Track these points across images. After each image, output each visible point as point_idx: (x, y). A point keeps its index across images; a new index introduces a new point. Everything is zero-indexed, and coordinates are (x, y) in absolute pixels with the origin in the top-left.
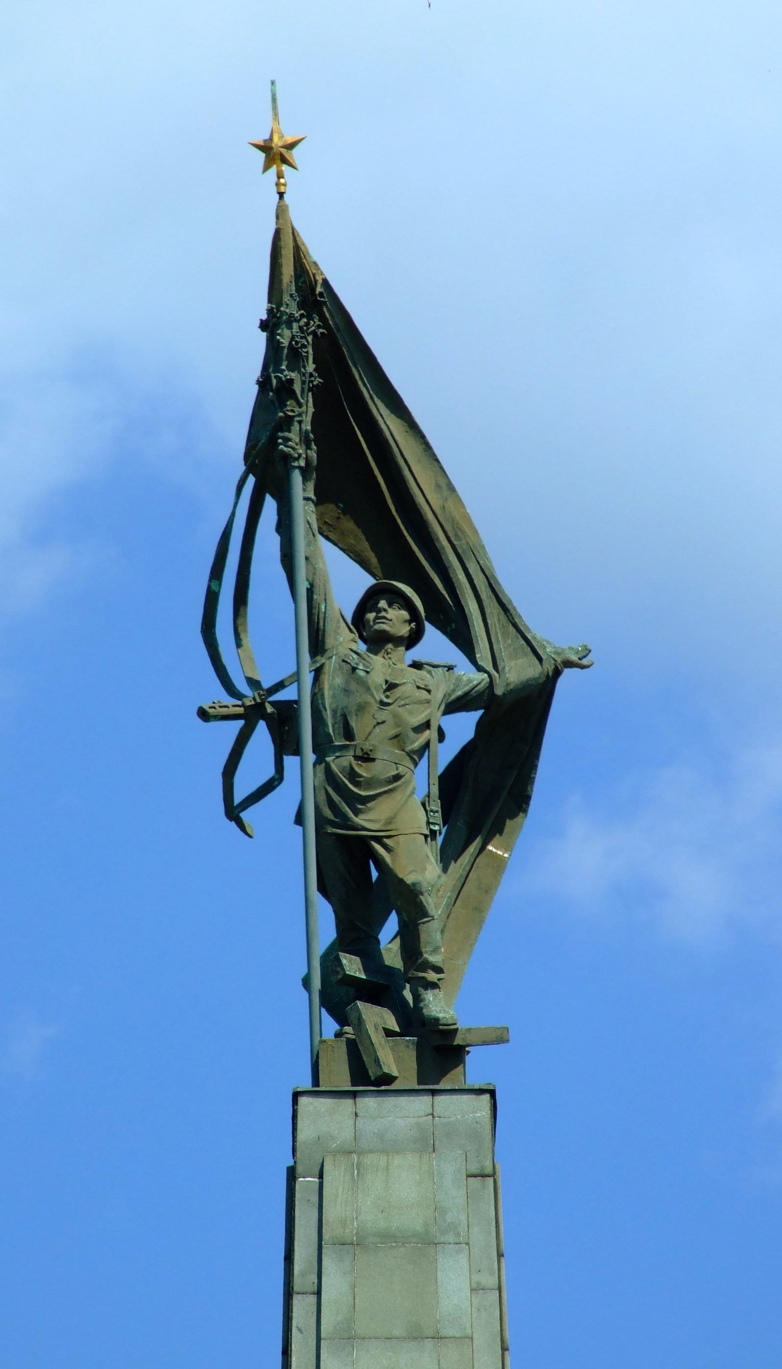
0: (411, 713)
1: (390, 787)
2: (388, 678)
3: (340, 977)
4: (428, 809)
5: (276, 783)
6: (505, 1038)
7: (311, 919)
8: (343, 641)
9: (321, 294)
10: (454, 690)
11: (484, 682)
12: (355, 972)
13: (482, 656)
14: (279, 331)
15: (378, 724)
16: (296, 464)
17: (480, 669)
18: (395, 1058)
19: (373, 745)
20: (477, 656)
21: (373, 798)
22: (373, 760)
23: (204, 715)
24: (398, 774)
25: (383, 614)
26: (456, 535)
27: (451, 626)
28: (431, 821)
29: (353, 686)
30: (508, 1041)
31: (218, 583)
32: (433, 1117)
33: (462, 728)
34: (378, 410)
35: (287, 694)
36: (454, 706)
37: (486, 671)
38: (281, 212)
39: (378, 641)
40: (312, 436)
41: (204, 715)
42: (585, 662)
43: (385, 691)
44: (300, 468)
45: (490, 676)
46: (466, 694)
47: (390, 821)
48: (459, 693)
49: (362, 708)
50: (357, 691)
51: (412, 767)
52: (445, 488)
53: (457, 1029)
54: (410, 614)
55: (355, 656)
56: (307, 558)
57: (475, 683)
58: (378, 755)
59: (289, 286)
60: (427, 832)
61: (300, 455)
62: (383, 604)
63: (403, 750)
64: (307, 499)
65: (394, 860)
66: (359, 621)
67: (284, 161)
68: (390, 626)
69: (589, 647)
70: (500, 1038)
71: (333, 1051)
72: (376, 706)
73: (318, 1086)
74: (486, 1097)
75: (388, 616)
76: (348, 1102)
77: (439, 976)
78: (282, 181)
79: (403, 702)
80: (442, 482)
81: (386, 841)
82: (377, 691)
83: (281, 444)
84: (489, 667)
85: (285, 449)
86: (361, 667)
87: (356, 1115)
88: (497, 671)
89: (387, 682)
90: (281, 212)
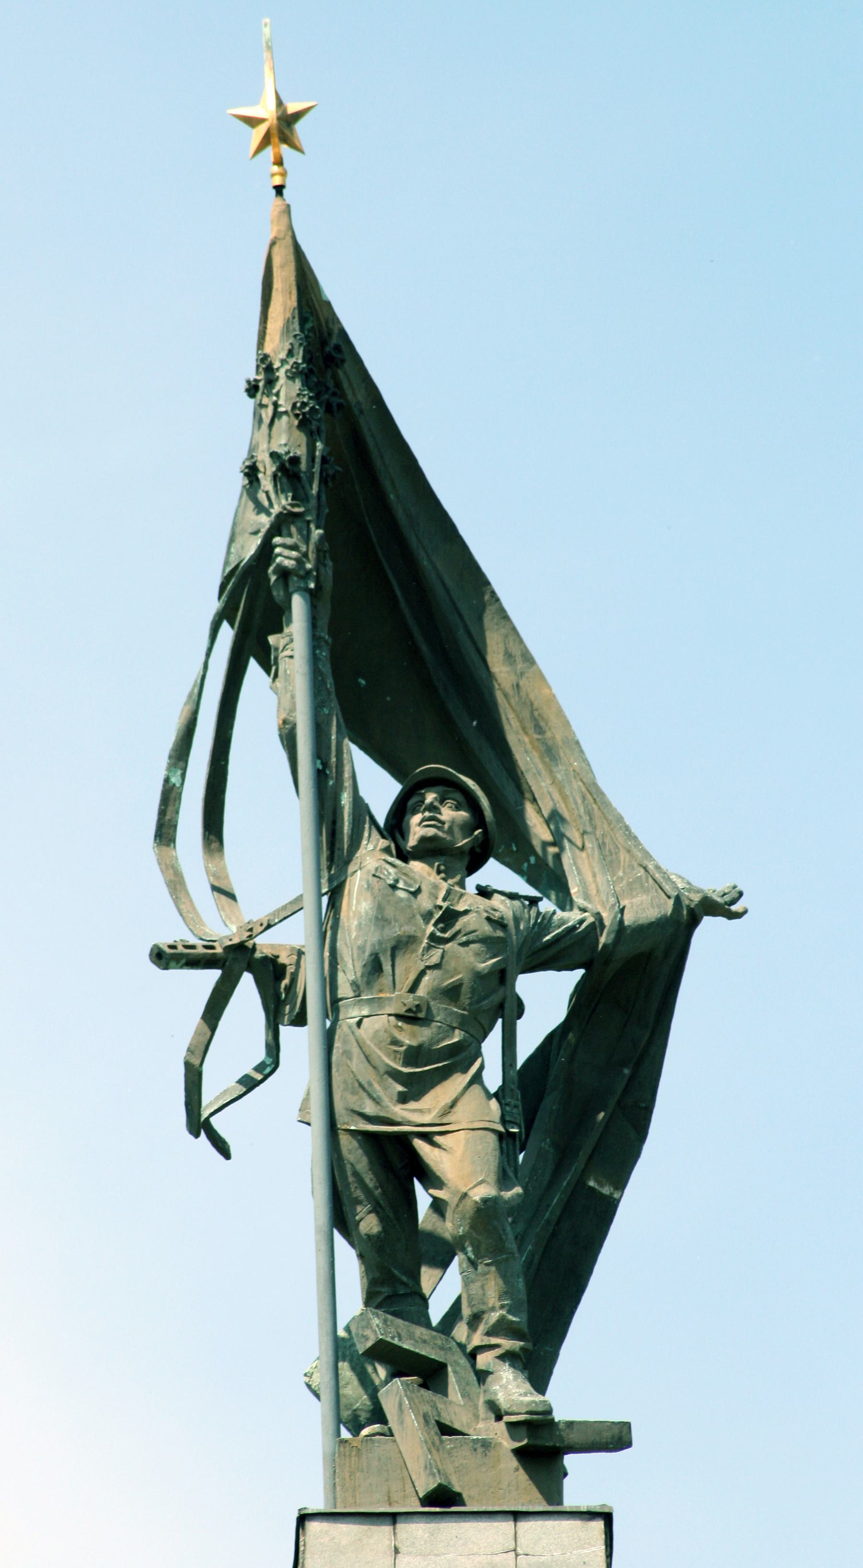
3: (369, 1344)
4: (503, 1101)
6: (625, 1439)
7: (325, 1267)
12: (393, 1338)
23: (162, 958)
27: (528, 861)
28: (507, 1118)
29: (389, 912)
32: (517, 1555)
50: (396, 921)
52: (519, 659)
70: (615, 1438)
74: (599, 1525)
76: (384, 1531)
79: (464, 939)
80: (516, 651)
81: (438, 1139)
87: (397, 1551)
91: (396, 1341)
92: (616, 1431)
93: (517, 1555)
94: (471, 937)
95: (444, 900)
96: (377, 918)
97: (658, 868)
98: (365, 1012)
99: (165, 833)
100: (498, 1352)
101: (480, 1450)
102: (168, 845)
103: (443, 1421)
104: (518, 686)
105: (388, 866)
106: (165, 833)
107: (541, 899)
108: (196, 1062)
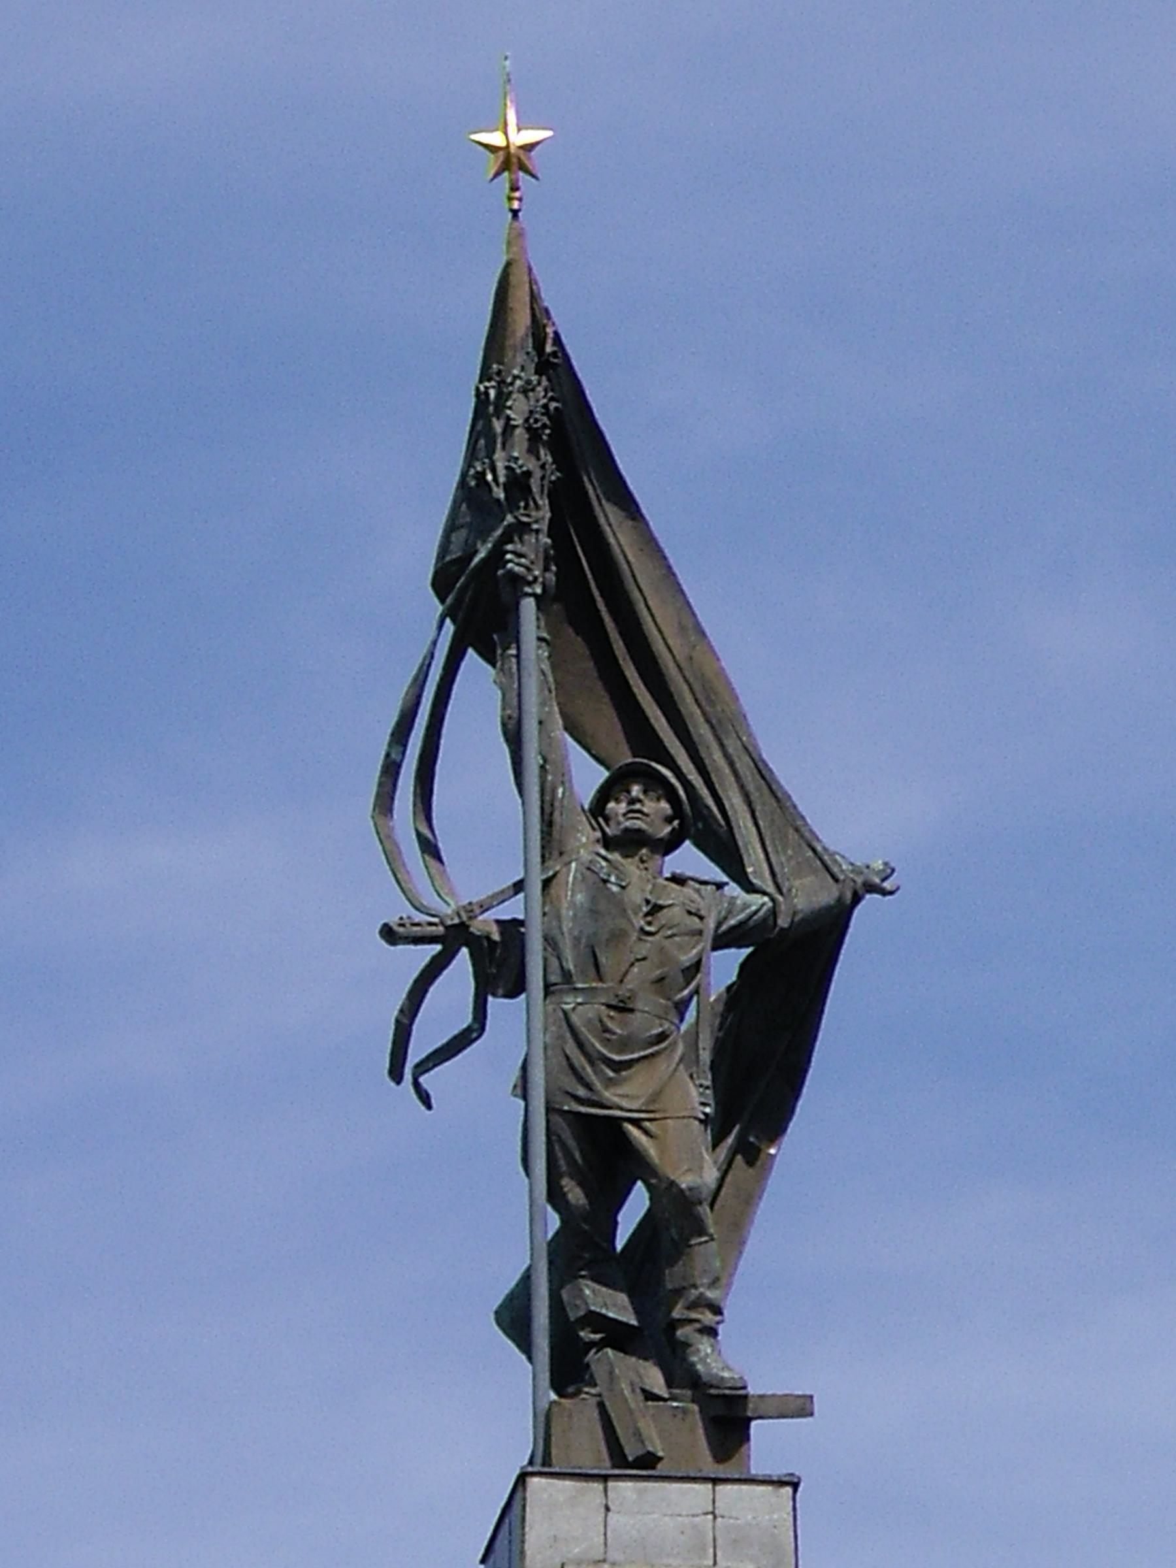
0: (680, 947)
1: (656, 1048)
2: (649, 897)
3: (582, 1313)
5: (475, 1035)
8: (583, 839)
9: (554, 354)
10: (725, 918)
11: (765, 908)
13: (755, 872)
14: (509, 403)
15: (638, 960)
16: (528, 590)
17: (750, 888)
18: (677, 1430)
19: (630, 990)
20: (750, 870)
21: (629, 1064)
22: (632, 1011)
23: (389, 934)
24: (663, 1032)
25: (638, 806)
26: (708, 698)
29: (603, 905)
30: (812, 1414)
31: (401, 749)
32: (715, 1517)
33: (725, 967)
34: (606, 516)
35: (512, 909)
36: (722, 941)
37: (765, 893)
38: (516, 238)
39: (629, 843)
40: (552, 552)
41: (389, 934)
42: (887, 885)
43: (647, 914)
44: (534, 595)
45: (773, 900)
46: (741, 924)
47: (655, 1097)
48: (733, 922)
49: (617, 937)
51: (677, 1021)
53: (746, 1397)
54: (672, 807)
55: (604, 864)
56: (540, 723)
57: (754, 908)
58: (639, 1005)
59: (524, 339)
60: (702, 1117)
61: (536, 578)
62: (636, 790)
63: (669, 999)
64: (540, 639)
65: (662, 1151)
66: (598, 810)
67: (523, 167)
68: (646, 823)
69: (893, 865)
71: (570, 1416)
72: (634, 936)
73: (550, 1466)
75: (645, 810)
77: (718, 1318)
78: (517, 194)
79: (669, 933)
81: (647, 1124)
82: (636, 914)
83: (510, 561)
84: (771, 889)
85: (517, 569)
86: (613, 879)
87: (607, 1509)
88: (781, 893)
89: (648, 902)
90: (516, 238)
91: (604, 1311)
92: (800, 1401)
93: (715, 1517)
94: (674, 931)
95: (651, 893)
96: (591, 911)
97: (825, 849)
98: (579, 1000)
99: (385, 802)
100: (698, 1326)
101: (680, 1416)
102: (386, 816)
103: (647, 1388)
104: (691, 658)
105: (600, 860)
106: (385, 802)
107: (727, 884)
108: (406, 1021)
